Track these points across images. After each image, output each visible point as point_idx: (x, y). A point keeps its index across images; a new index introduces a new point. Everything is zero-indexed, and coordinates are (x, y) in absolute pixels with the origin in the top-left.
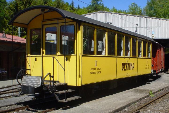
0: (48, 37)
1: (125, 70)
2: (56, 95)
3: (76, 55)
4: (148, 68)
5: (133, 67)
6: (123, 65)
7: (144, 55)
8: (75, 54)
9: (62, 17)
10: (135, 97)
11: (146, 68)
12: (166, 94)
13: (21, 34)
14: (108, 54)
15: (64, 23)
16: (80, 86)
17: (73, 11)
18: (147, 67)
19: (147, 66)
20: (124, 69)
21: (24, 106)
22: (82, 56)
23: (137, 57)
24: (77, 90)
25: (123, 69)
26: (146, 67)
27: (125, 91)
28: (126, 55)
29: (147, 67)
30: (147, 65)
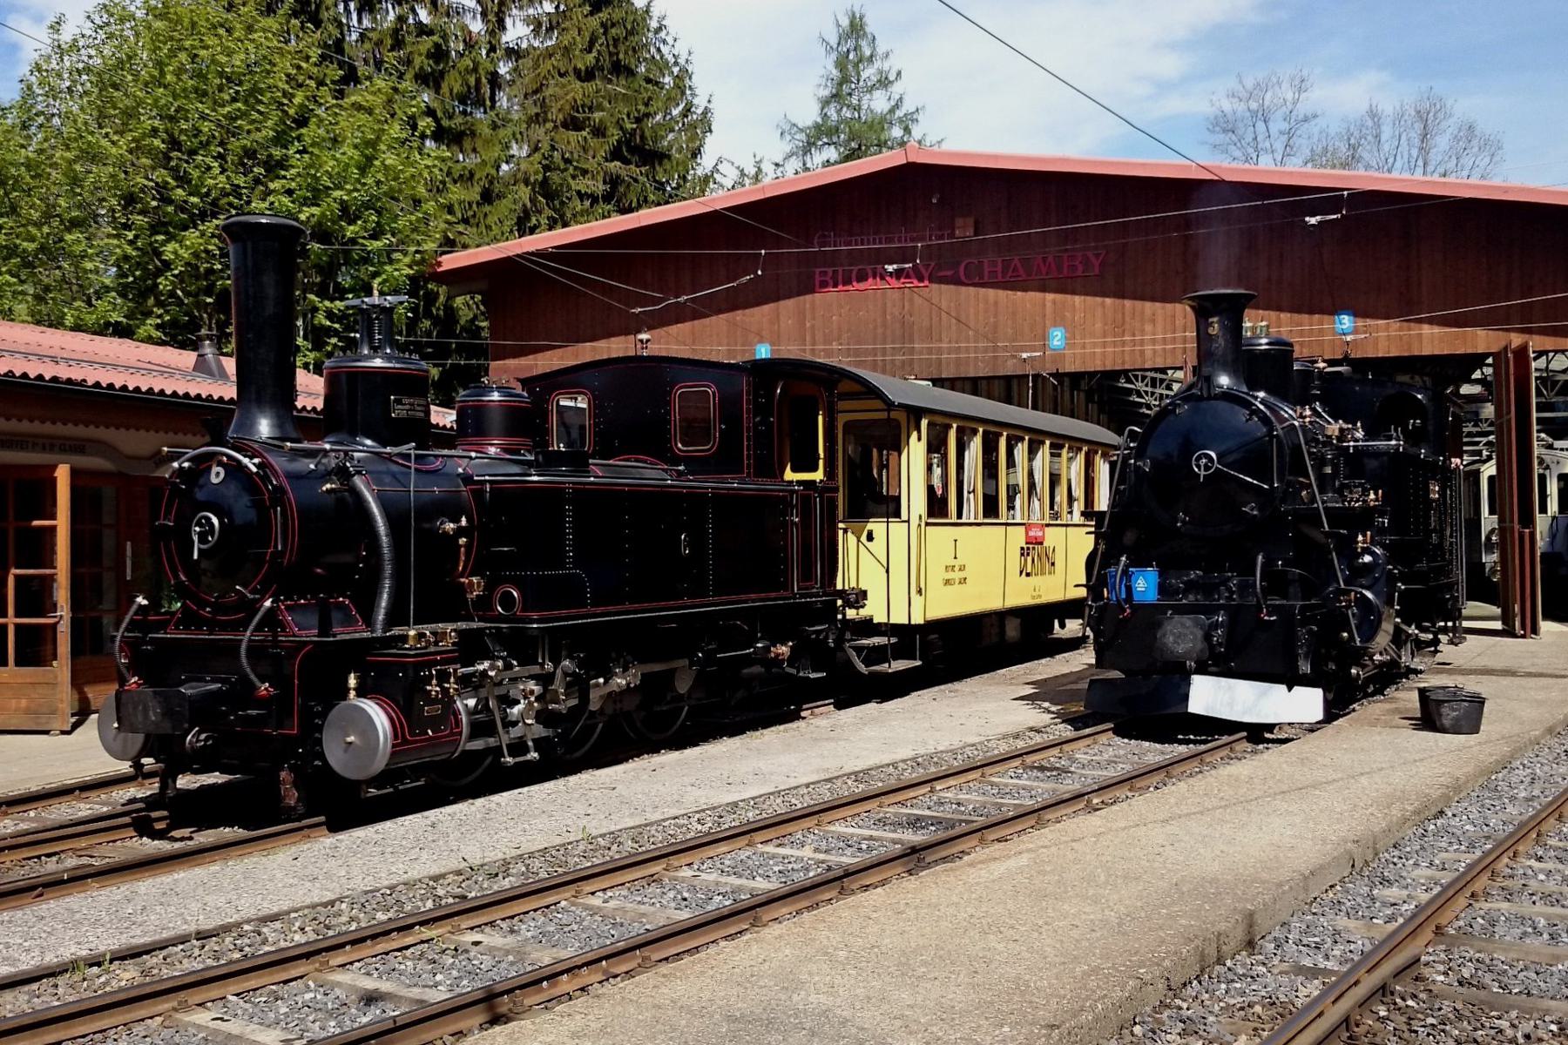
0: (675, 421)
1: (1028, 575)
2: (853, 654)
3: (908, 521)
4: (957, 582)
5: (1053, 564)
6: (1022, 554)
7: (991, 508)
8: (904, 516)
9: (863, 389)
10: (195, 1016)
11: (947, 582)
12: (599, 960)
13: (684, 424)
14: (985, 516)
15: (886, 413)
16: (919, 625)
17: (404, 135)
18: (957, 575)
19: (957, 569)
20: (1024, 573)
21: (460, 749)
22: (927, 524)
23: (954, 520)
24: (906, 637)
25: (1021, 573)
26: (950, 575)
27: (626, 760)
28: (960, 516)
29: (957, 575)
30: (957, 563)
